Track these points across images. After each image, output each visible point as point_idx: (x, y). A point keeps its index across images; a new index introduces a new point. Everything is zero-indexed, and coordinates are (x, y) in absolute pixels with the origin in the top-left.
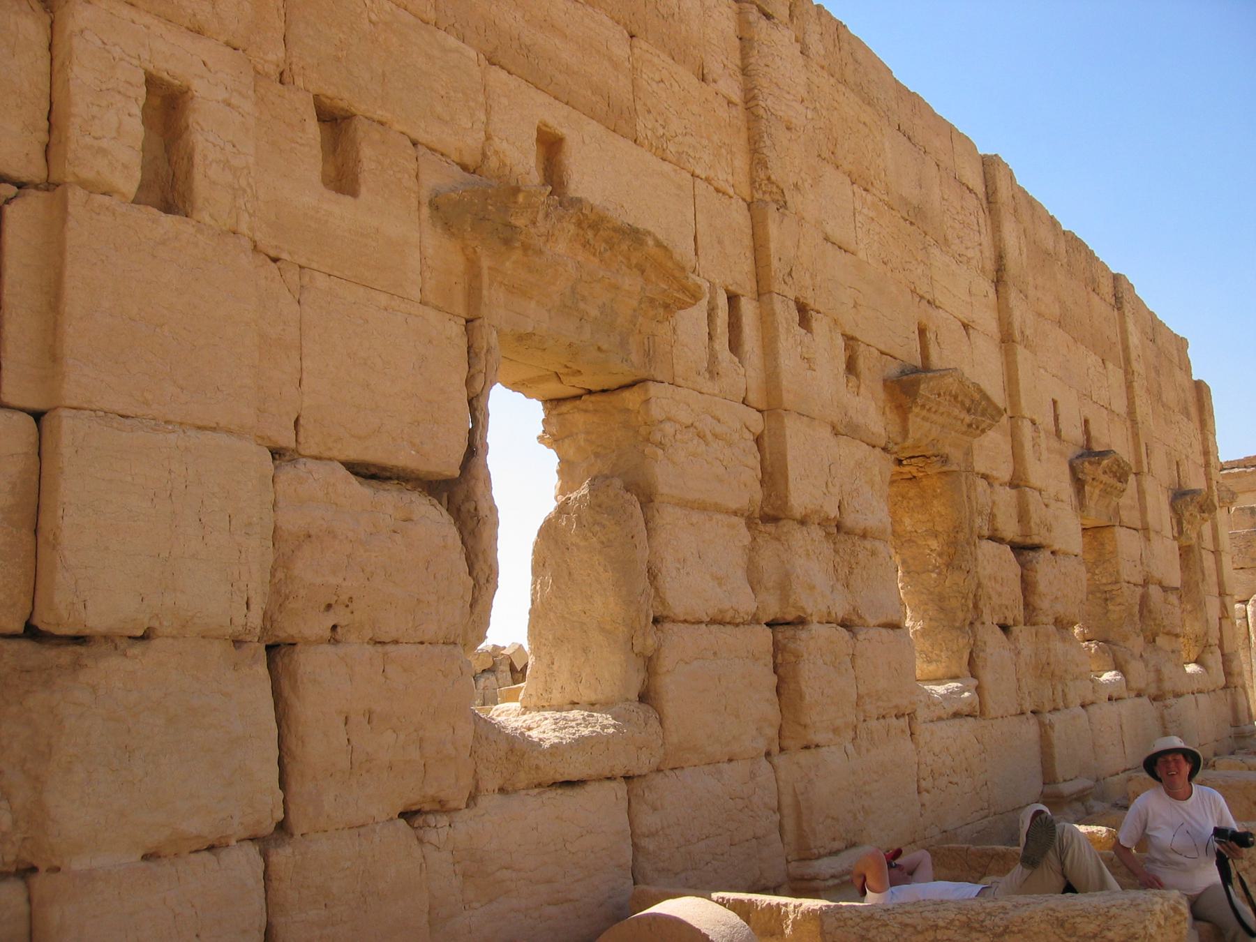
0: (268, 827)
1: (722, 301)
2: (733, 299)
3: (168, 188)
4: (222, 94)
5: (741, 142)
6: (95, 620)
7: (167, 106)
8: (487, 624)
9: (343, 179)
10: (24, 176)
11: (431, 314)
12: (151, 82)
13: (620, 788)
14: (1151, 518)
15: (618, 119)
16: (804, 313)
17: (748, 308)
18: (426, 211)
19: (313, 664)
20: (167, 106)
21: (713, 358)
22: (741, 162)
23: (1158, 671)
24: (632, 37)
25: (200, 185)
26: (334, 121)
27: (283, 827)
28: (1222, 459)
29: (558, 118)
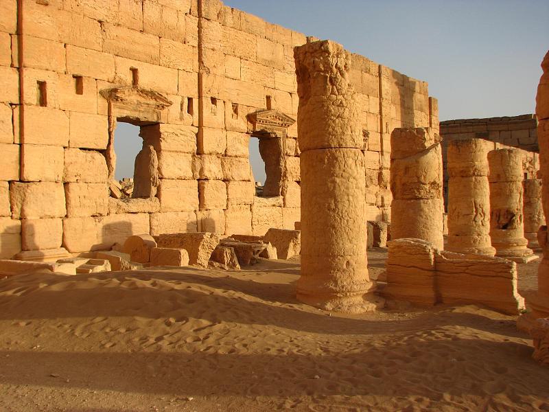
0: (64, 216)
1: (186, 101)
2: (190, 100)
3: (43, 102)
4: (52, 82)
5: (197, 57)
6: (31, 179)
7: (42, 85)
8: (536, 108)
9: (79, 90)
10: (16, 103)
11: (100, 116)
12: (38, 82)
13: (147, 215)
14: (384, 148)
15: (154, 61)
16: (214, 100)
17: (195, 102)
18: (99, 94)
19: (71, 186)
20: (42, 85)
21: (182, 115)
22: (196, 63)
23: (382, 198)
24: (160, 38)
25: (48, 100)
26: (78, 79)
27: (66, 216)
28: (532, 111)
29: (135, 65)
